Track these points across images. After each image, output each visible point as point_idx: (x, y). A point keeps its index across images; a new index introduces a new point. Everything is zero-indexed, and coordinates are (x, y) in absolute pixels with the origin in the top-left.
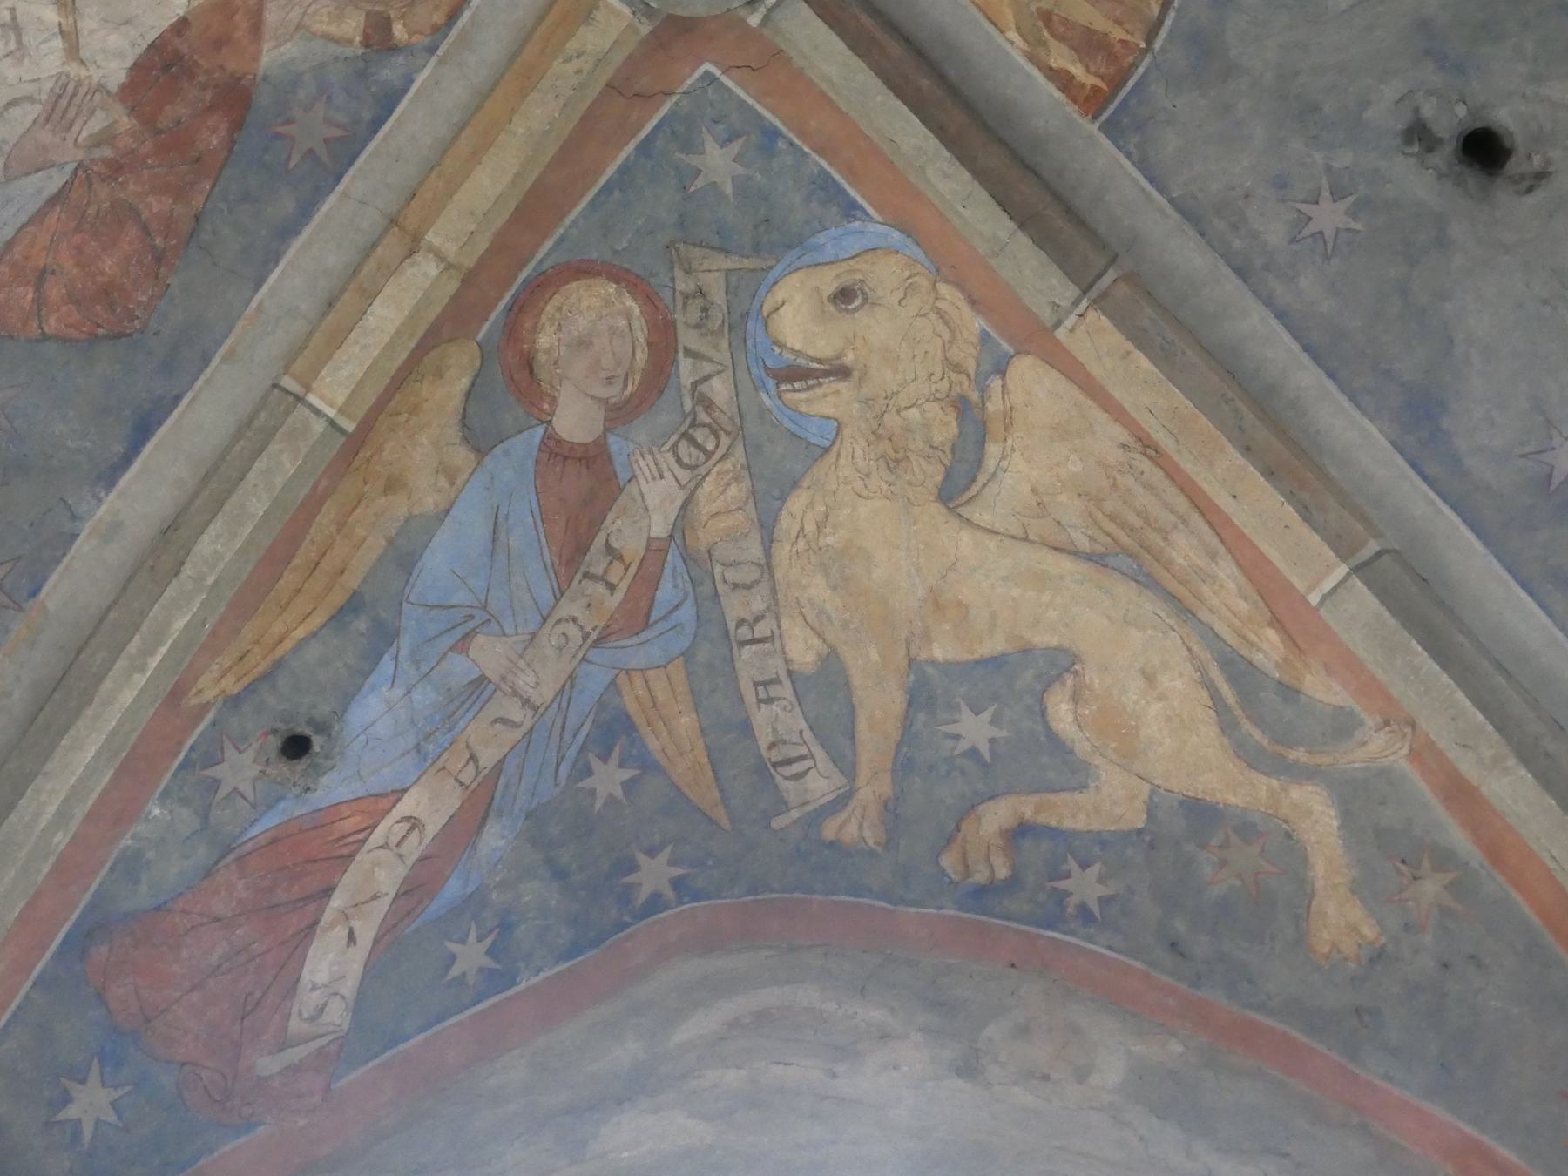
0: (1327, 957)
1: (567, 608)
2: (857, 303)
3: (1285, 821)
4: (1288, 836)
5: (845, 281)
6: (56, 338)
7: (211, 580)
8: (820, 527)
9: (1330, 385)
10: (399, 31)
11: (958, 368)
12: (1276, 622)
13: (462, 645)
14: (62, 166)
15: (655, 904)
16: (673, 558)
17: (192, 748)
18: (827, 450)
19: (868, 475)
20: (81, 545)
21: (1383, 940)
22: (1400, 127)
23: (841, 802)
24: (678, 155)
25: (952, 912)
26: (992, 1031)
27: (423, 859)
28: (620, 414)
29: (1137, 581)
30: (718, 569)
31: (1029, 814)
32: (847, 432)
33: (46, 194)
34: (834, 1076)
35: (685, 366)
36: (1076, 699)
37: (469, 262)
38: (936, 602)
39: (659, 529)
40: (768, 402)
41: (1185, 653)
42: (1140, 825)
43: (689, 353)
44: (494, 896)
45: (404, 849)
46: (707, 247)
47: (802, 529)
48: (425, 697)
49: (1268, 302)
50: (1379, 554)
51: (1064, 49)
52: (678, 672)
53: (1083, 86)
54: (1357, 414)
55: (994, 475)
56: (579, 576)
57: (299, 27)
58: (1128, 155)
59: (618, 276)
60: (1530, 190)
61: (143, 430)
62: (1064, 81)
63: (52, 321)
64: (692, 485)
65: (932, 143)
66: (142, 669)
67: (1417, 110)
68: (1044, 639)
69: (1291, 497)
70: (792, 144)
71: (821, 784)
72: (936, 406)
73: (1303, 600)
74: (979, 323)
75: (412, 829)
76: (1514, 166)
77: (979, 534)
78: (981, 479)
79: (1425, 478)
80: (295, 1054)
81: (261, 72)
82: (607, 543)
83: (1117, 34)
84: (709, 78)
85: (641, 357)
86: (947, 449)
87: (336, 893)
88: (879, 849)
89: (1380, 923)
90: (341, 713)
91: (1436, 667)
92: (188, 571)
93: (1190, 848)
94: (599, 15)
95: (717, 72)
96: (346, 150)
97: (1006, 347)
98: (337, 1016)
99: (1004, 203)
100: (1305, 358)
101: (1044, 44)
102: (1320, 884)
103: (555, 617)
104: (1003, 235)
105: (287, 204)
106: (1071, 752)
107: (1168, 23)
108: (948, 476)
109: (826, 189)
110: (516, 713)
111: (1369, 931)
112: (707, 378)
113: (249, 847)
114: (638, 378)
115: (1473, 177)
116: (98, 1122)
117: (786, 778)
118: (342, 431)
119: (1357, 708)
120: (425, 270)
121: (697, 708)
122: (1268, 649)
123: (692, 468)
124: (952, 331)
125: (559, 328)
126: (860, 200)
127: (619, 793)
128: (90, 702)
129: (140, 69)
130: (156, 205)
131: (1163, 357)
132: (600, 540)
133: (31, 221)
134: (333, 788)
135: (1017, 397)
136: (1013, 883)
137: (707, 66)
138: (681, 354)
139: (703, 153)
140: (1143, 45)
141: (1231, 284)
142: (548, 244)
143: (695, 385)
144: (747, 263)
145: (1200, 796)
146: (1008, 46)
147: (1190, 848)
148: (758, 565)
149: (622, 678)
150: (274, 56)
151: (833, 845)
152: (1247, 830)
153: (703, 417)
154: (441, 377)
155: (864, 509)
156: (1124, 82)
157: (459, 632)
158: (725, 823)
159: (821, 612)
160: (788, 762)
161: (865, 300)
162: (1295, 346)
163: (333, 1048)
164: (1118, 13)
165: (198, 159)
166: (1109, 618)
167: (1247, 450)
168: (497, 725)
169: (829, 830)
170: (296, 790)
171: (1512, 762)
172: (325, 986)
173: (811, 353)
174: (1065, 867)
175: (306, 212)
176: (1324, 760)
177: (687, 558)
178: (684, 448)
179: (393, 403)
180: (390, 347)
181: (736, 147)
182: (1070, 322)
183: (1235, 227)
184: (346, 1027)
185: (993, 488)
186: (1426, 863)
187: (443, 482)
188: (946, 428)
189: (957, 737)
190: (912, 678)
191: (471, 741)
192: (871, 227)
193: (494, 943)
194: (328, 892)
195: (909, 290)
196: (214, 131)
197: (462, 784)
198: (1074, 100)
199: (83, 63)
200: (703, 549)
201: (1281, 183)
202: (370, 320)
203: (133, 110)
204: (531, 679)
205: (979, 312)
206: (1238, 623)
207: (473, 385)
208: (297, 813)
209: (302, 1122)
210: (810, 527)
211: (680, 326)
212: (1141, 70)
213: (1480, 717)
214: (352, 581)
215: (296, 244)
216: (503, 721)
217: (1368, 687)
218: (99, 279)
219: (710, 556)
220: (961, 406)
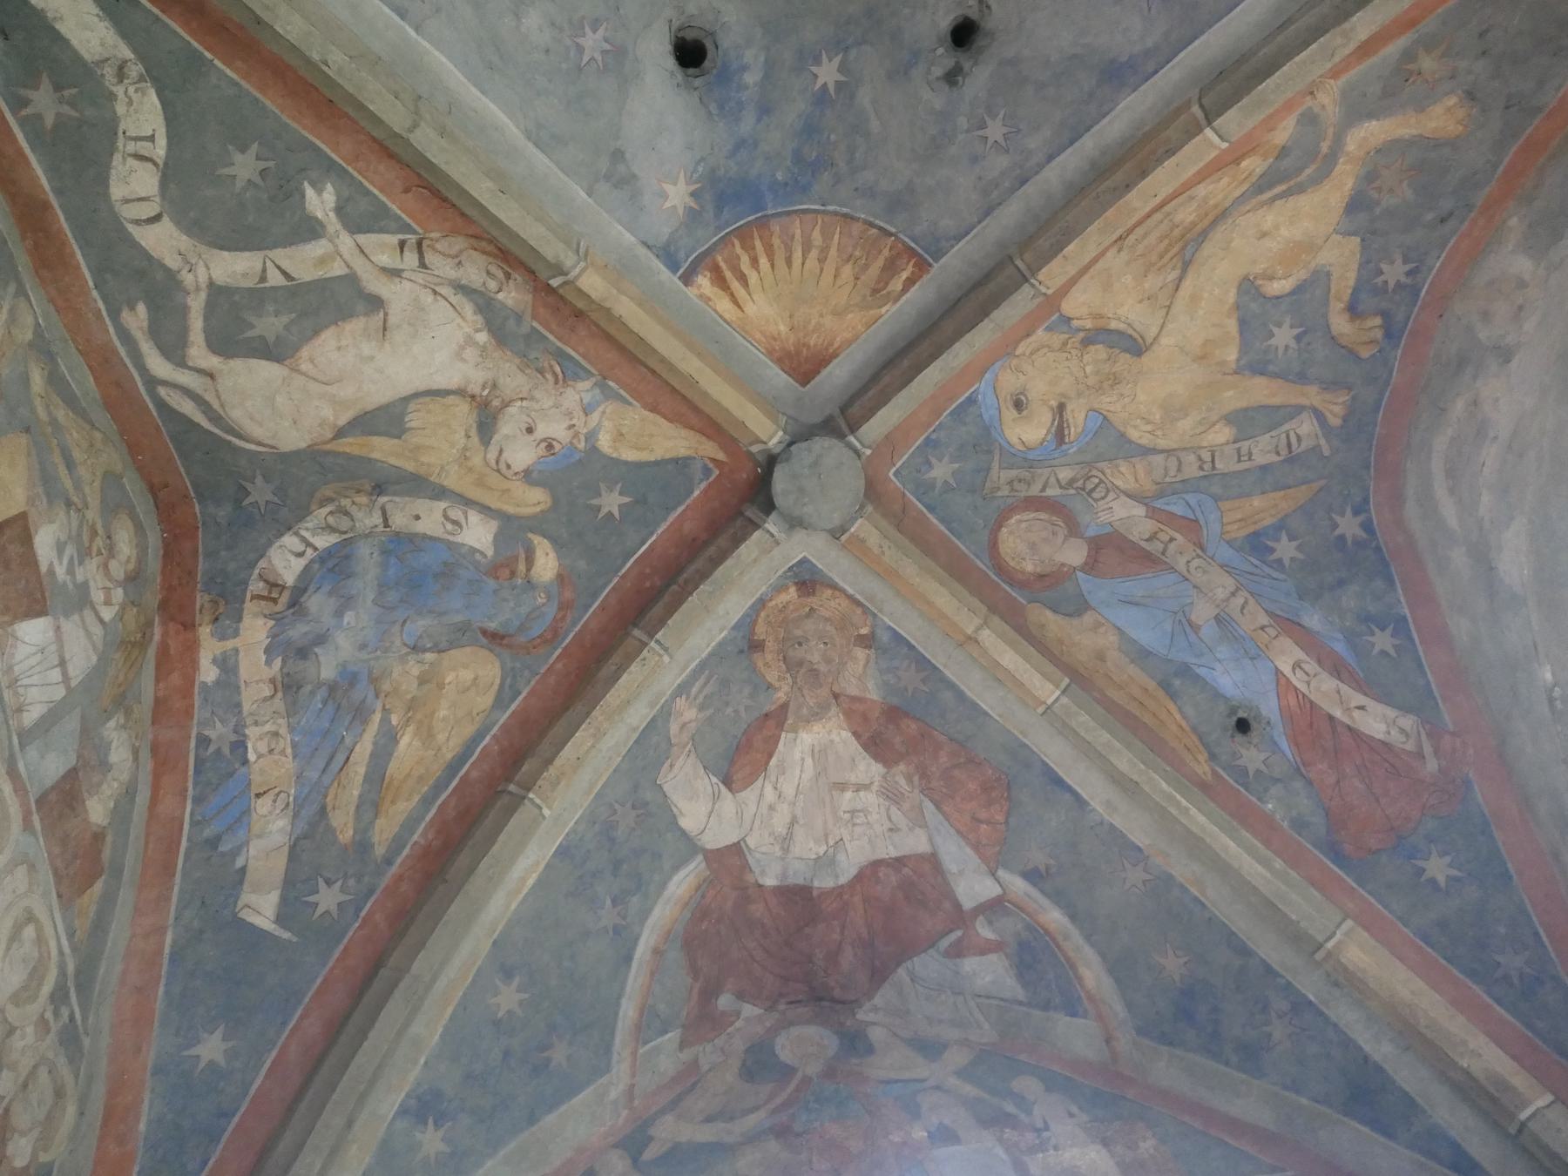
0: (1466, 126)
1: (1181, 566)
2: (1023, 398)
3: (1369, 153)
4: (1378, 151)
5: (1010, 405)
6: (1007, 818)
7: (1142, 767)
8: (1149, 422)
9: (1097, 128)
10: (864, 631)
11: (1065, 344)
12: (1237, 161)
13: (1195, 628)
14: (921, 801)
15: (1368, 527)
16: (1158, 504)
17: (1236, 782)
18: (1105, 417)
19: (1122, 395)
20: (1117, 822)
21: (1460, 92)
22: (947, 88)
23: (1319, 416)
24: (936, 491)
25: (1400, 351)
26: (1483, 334)
27: (1319, 662)
28: (1074, 529)
29: (1203, 242)
30: (1168, 479)
31: (1342, 305)
32: (1096, 406)
33: (935, 811)
34: (1496, 438)
35: (1049, 492)
36: (1271, 278)
37: (984, 609)
38: (1202, 358)
39: (1140, 511)
40: (1075, 449)
41: (1251, 214)
42: (1358, 240)
43: (1043, 490)
44: (1348, 624)
45: (1312, 673)
46: (986, 478)
47: (1149, 432)
48: (1223, 651)
49: (1041, 167)
50: (1201, 106)
51: (893, 282)
52: (1225, 505)
53: (913, 273)
54: (1113, 113)
55: (1129, 324)
56: (1163, 558)
57: (860, 680)
58: (952, 246)
59: (999, 525)
60: (988, 7)
61: (1059, 782)
62: (910, 282)
63: (997, 817)
64: (1118, 492)
65: (938, 363)
66: (1187, 809)
67: (938, 79)
68: (1232, 297)
69: (1160, 161)
70: (934, 431)
71: (1306, 427)
72: (1086, 357)
73: (1225, 151)
74: (1040, 332)
75: (1300, 667)
76: (974, 14)
77: (1163, 333)
78: (1130, 331)
79: (1156, 72)
80: (1428, 749)
81: (881, 700)
82: (1147, 540)
83: (886, 252)
84: (896, 474)
85: (1043, 516)
86: (1111, 351)
87: (1331, 712)
88: (1352, 393)
89: (1447, 94)
90: (1226, 699)
91: (1278, 73)
92: (1135, 777)
93: (1378, 211)
94: (862, 536)
95: (894, 469)
96: (922, 663)
97: (1054, 317)
98: (1408, 722)
99: (972, 325)
100: (1077, 144)
101: (889, 293)
102: (1414, 132)
103: (1186, 573)
104: (992, 325)
105: (947, 695)
106: (1305, 280)
107: (882, 224)
108: (1127, 351)
109: (959, 413)
110: (1239, 601)
111: (1452, 101)
112: (1058, 480)
113: (1298, 759)
114: (1054, 518)
115: (980, 41)
116: (1450, 865)
117: (1299, 445)
118: (1069, 685)
119: (1300, 111)
120: (986, 636)
121: (1249, 495)
122: (1254, 165)
123: (1108, 491)
124: (1043, 347)
125: (1024, 559)
126: (966, 395)
127: (1294, 544)
128: (1203, 839)
129: (877, 757)
130: (944, 759)
131: (1069, 235)
132: (1143, 544)
133: (948, 820)
134: (1269, 707)
135: (1084, 311)
136: (1385, 314)
137: (891, 474)
138: (1043, 494)
139: (935, 479)
140: (893, 238)
141: (1029, 188)
142: (979, 563)
143: (1061, 487)
144: (997, 457)
145: (1344, 205)
146: (889, 313)
147: (1378, 211)
148: (1168, 458)
149: (1227, 537)
150: (874, 694)
151: (1345, 420)
152: (1370, 177)
153: (1080, 484)
154: (1043, 625)
155: (1142, 397)
156: (913, 249)
157: (1188, 629)
158: (1322, 482)
159: (1200, 423)
160: (1289, 445)
161: (1021, 393)
162: (1070, 150)
163: (1427, 727)
164: (875, 252)
165: (923, 736)
166: (1223, 259)
167: (1128, 187)
168: (1245, 611)
169: (1335, 422)
170: (1268, 729)
171: (1346, 25)
172: (1388, 727)
173: (1049, 424)
174: (1380, 284)
175: (951, 686)
176: (1330, 131)
177: (1160, 495)
178: (1095, 495)
179: (1056, 652)
180: (1026, 658)
181: (933, 460)
182: (1043, 290)
183: (997, 186)
184: (1416, 718)
185: (1137, 325)
186: (1410, 66)
187: (1102, 630)
188: (1099, 351)
189: (1287, 347)
190: (1246, 372)
191: (1252, 628)
192: (981, 390)
193: (1378, 627)
194: (1331, 718)
195: (1019, 370)
196: (908, 726)
197: (1277, 636)
198: (921, 277)
199: (872, 783)
200: (1155, 487)
201: (975, 159)
202: (1011, 667)
203: (896, 763)
204: (1220, 590)
205: (1034, 331)
206: (1235, 183)
207: (1051, 609)
208: (1282, 730)
209: (1471, 751)
210: (1149, 428)
211: (1030, 493)
212: (907, 240)
213: (1314, 46)
214: (1152, 685)
215: (969, 693)
216: (1243, 608)
217: (1289, 106)
218: (979, 792)
219: (1159, 483)
220: (1087, 342)
